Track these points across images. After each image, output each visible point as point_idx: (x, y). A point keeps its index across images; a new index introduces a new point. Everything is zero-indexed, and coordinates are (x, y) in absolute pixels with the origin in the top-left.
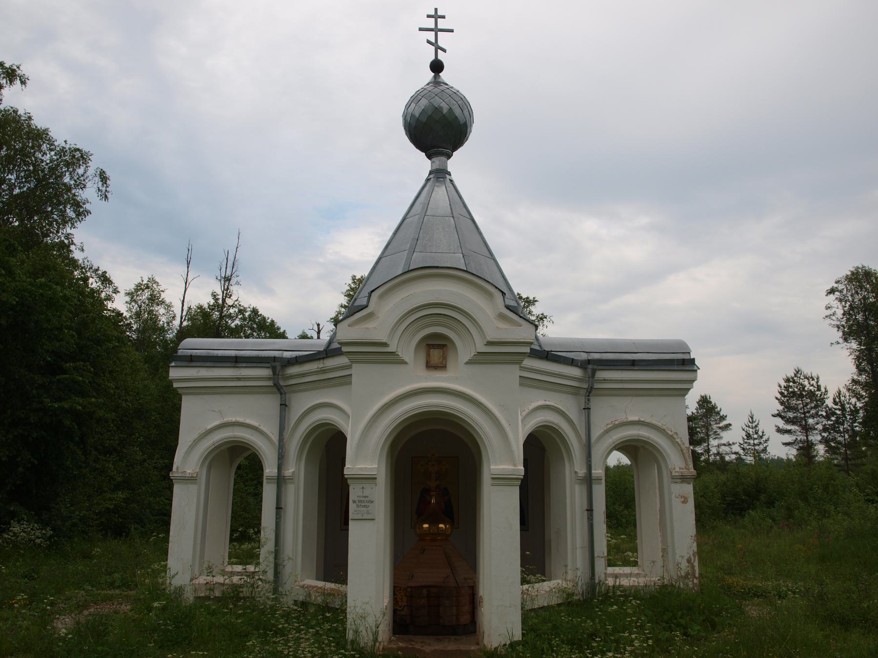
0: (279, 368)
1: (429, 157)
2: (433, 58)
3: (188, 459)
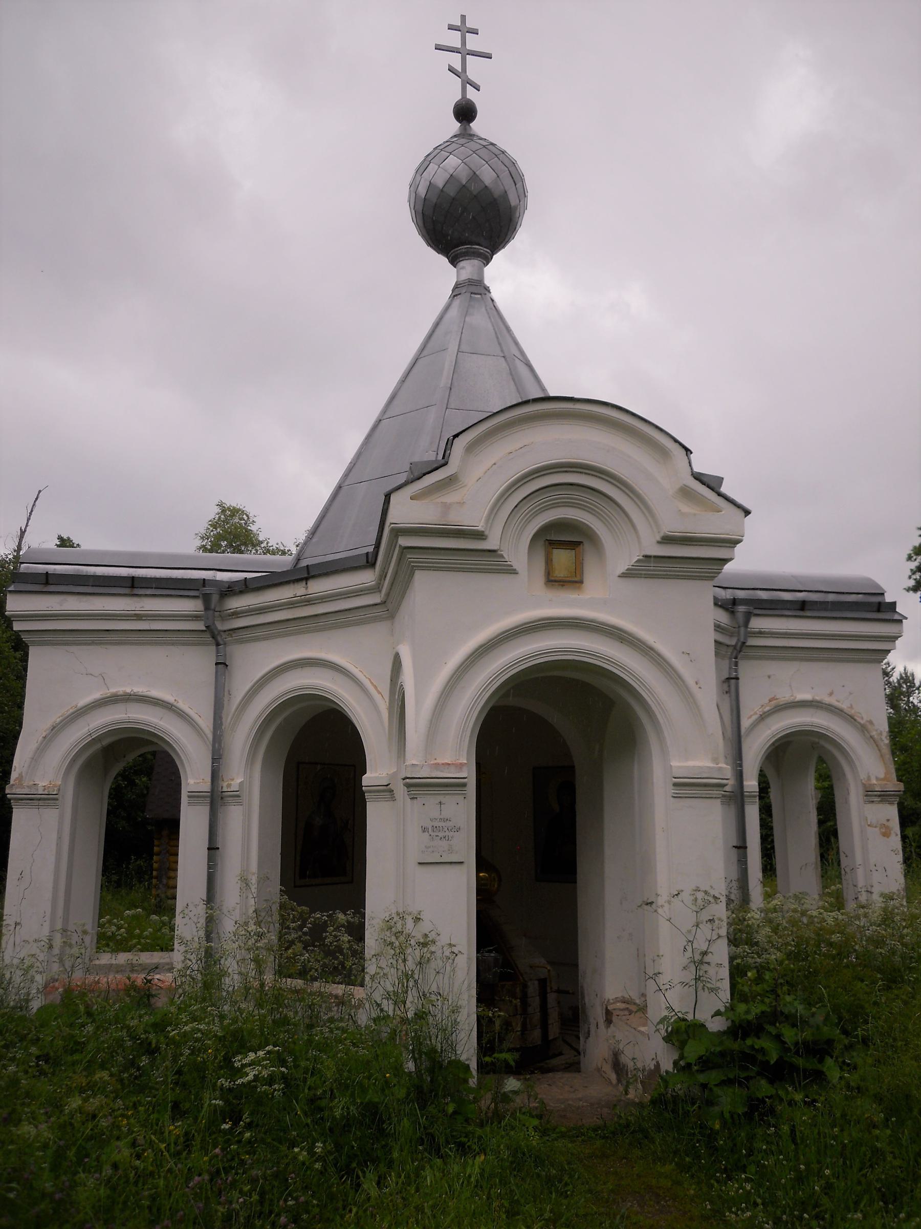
0: (215, 598)
1: (454, 261)
2: (459, 97)
3: (44, 759)
